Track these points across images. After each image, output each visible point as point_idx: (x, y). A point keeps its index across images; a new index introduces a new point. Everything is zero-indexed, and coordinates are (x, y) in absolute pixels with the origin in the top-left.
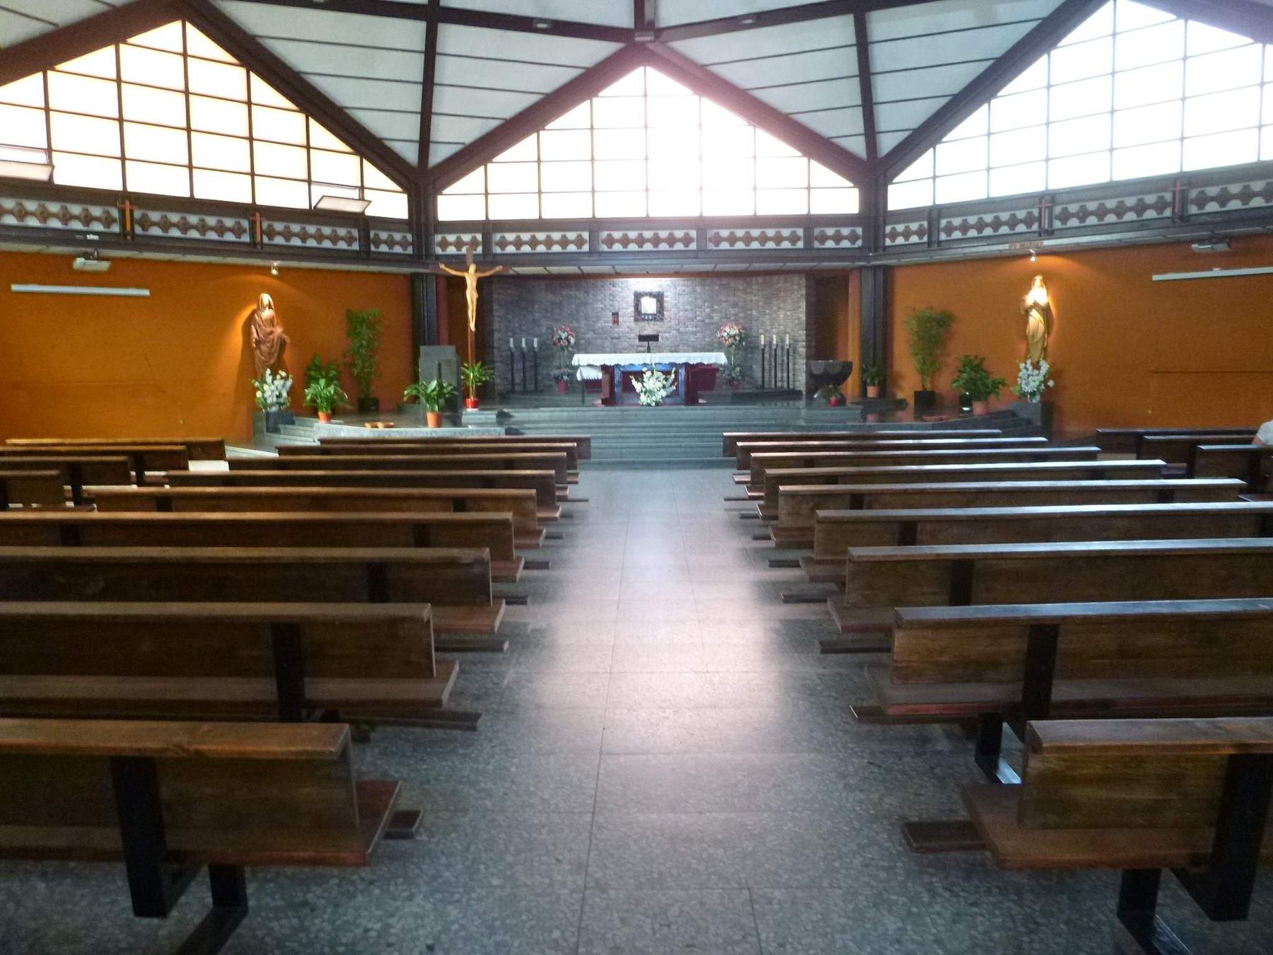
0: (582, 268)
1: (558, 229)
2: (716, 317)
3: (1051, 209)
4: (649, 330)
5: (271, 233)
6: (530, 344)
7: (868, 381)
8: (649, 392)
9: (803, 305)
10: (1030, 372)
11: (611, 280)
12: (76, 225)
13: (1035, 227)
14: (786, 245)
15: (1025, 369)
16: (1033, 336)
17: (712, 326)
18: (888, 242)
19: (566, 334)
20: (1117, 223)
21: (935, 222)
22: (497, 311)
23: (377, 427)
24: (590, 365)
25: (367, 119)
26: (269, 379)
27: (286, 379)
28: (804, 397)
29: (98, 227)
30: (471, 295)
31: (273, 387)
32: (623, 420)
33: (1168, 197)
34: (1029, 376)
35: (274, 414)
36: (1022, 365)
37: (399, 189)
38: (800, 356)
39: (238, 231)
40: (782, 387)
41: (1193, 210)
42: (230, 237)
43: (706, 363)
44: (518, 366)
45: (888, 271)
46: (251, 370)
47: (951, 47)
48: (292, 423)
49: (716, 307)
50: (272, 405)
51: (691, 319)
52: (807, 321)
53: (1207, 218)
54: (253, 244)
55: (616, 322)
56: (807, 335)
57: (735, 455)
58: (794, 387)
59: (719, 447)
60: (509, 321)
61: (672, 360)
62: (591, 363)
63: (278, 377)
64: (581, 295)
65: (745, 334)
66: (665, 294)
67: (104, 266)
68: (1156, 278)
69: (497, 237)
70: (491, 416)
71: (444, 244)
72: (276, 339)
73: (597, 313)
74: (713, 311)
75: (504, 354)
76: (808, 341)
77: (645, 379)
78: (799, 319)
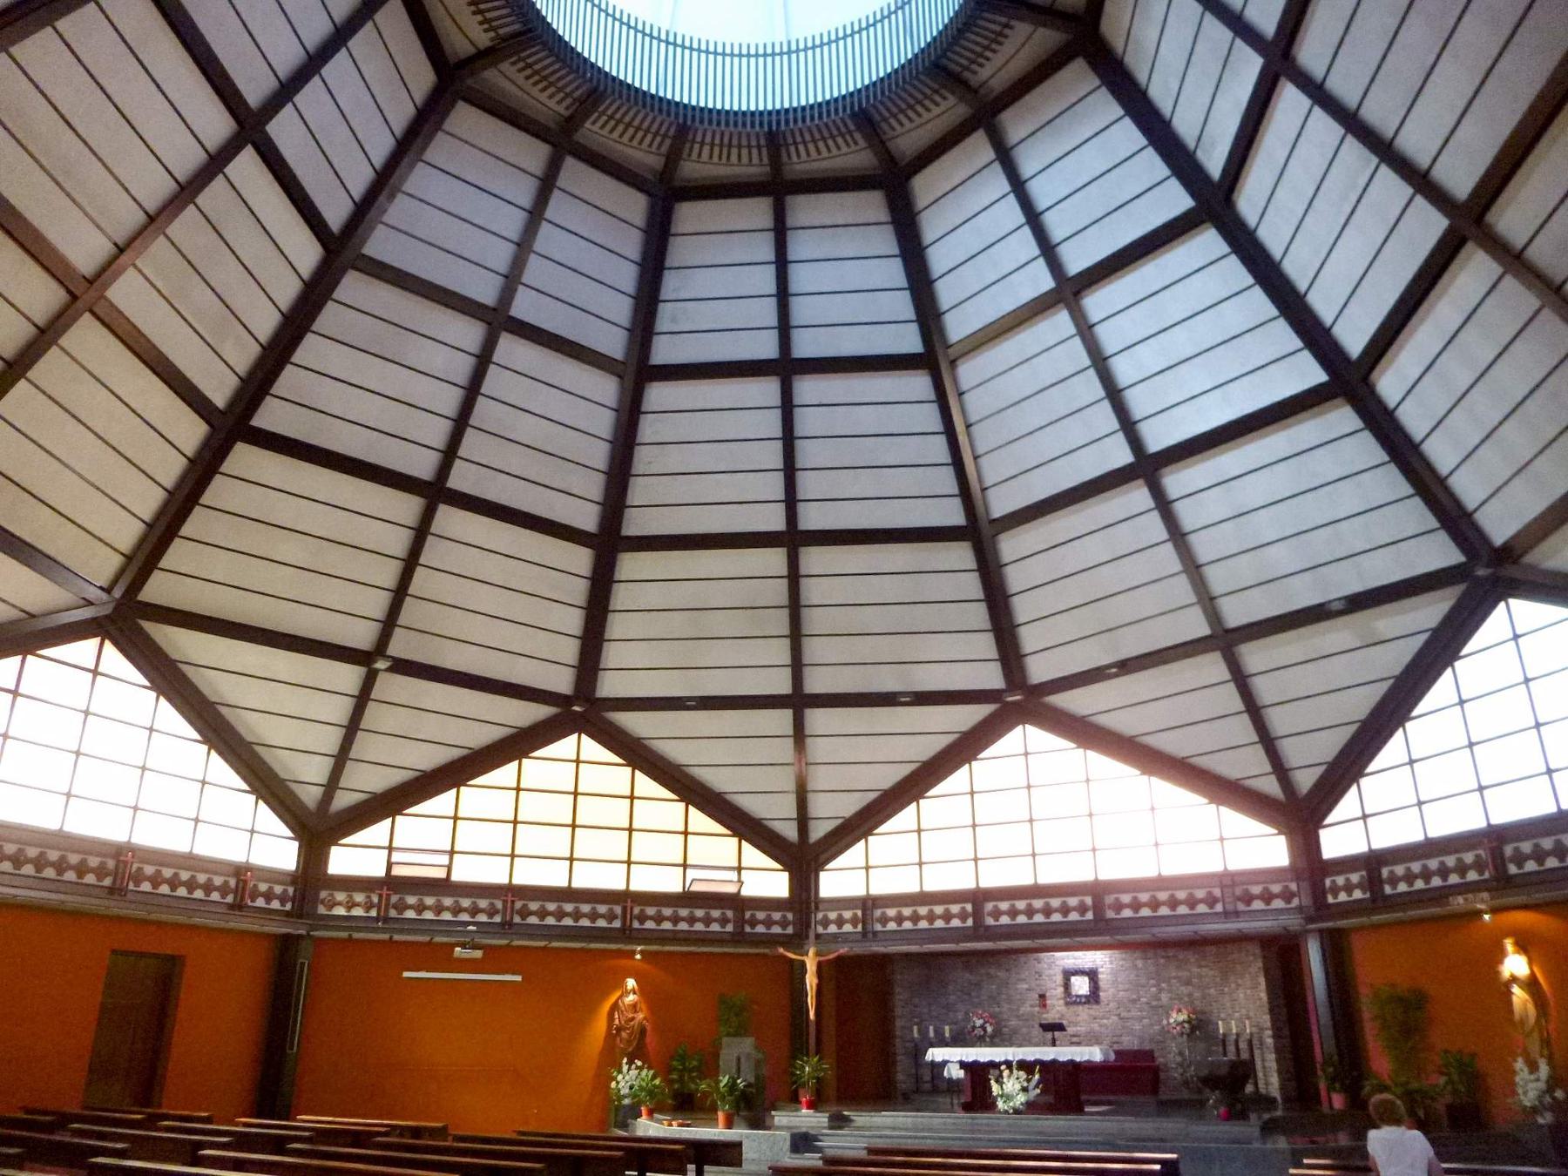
5: (642, 918)
8: (1008, 1098)
9: (1262, 980)
11: (1036, 955)
19: (981, 1021)
22: (899, 994)
25: (746, 803)
27: (640, 1068)
28: (1280, 1107)
30: (811, 981)
37: (779, 866)
38: (1267, 1048)
39: (611, 917)
42: (602, 923)
43: (1078, 1060)
46: (609, 1061)
50: (625, 1097)
51: (1134, 1001)
54: (623, 930)
60: (916, 1006)
61: (1038, 1057)
63: (633, 1066)
64: (1002, 974)
65: (1197, 1018)
66: (1100, 970)
67: (478, 954)
73: (1021, 994)
78: (1261, 999)
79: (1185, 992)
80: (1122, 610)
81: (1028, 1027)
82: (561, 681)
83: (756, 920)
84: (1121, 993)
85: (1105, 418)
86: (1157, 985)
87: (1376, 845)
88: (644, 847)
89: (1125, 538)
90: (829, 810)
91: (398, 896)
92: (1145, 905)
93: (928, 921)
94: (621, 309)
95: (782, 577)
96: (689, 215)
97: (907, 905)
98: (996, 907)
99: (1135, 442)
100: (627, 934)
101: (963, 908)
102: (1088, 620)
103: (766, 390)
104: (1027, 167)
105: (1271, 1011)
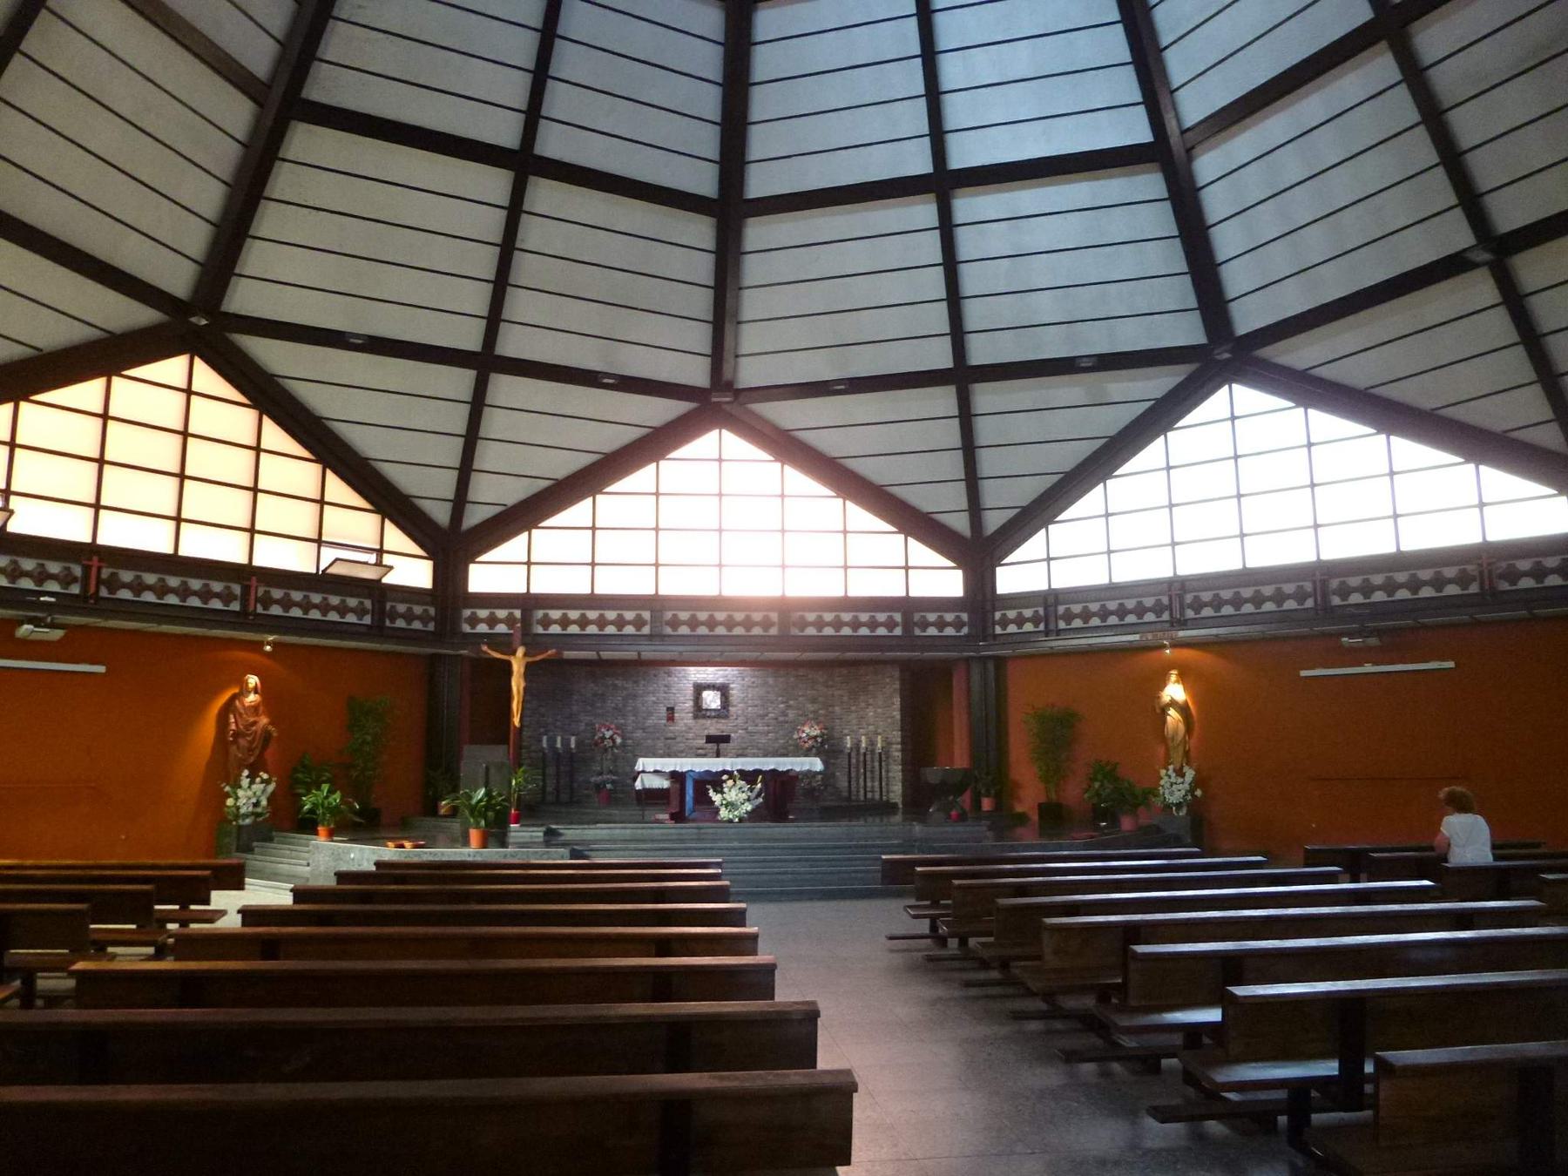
0: (601, 653)
1: (614, 608)
2: (791, 714)
3: (1181, 598)
4: (714, 728)
5: (267, 601)
6: (566, 743)
7: (983, 791)
8: (730, 805)
9: (897, 701)
10: (1173, 780)
11: (666, 669)
12: (26, 584)
13: (1166, 616)
14: (882, 631)
15: (1167, 777)
16: (1173, 739)
17: (786, 725)
18: (998, 630)
20: (1156, 622)
21: (1052, 609)
23: (402, 846)
24: (656, 772)
25: (394, 474)
26: (245, 782)
27: (267, 782)
28: (901, 811)
29: (54, 587)
31: (250, 793)
32: (699, 840)
33: (1308, 586)
34: (1172, 785)
35: (247, 826)
36: (1163, 772)
39: (227, 597)
40: (873, 799)
41: (1336, 601)
42: (216, 604)
44: (551, 770)
45: (1000, 662)
46: (223, 770)
47: (1061, 424)
48: (271, 840)
49: (791, 702)
50: (246, 816)
51: (763, 716)
52: (902, 720)
53: (1352, 610)
54: (244, 613)
55: (671, 718)
56: (903, 737)
57: (896, 879)
58: (888, 801)
59: (875, 871)
62: (658, 769)
63: (258, 780)
64: (629, 685)
66: (732, 686)
67: (57, 634)
68: (1304, 673)
70: (538, 833)
71: (474, 621)
72: (259, 732)
74: (789, 707)
75: (533, 755)
76: (903, 743)
77: (726, 790)
80: (869, 326)
81: (653, 739)
82: (178, 279)
84: (750, 709)
88: (271, 513)
89: (893, 252)
90: (1002, 501)
91: (110, 570)
95: (1451, 208)
97: (29, 555)
98: (674, 615)
99: (939, 152)
102: (826, 330)
105: (902, 730)
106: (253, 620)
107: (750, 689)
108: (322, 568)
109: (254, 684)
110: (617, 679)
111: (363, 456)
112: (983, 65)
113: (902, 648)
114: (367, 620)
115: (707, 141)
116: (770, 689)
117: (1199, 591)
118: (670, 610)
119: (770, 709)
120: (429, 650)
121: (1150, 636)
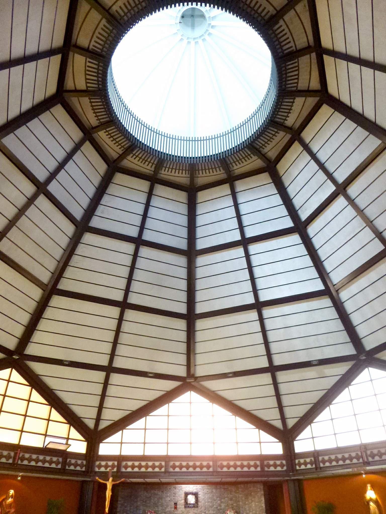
2: (223, 506)
9: (263, 499)
13: (361, 460)
18: (298, 468)
21: (317, 458)
22: (120, 501)
30: (108, 493)
47: (309, 385)
51: (211, 507)
55: (176, 508)
64: (160, 493)
66: (199, 493)
69: (124, 463)
74: (221, 502)
78: (262, 507)
79: (230, 503)
80: (238, 353)
83: (101, 465)
85: (248, 286)
86: (220, 500)
87: (170, 454)
89: (245, 329)
92: (239, 466)
93: (131, 468)
94: (85, 202)
96: (119, 178)
98: (174, 464)
100: (14, 466)
101: (161, 464)
102: (225, 355)
103: (130, 248)
104: (240, 199)
106: (16, 466)
107: (206, 494)
108: (45, 445)
109: (12, 494)
110: (155, 491)
111: (66, 403)
112: (267, 270)
113: (261, 476)
114: (59, 466)
115: (183, 297)
116: (214, 495)
117: (372, 449)
118: (321, 456)
119: (214, 503)
120: (83, 479)
121: (356, 469)
